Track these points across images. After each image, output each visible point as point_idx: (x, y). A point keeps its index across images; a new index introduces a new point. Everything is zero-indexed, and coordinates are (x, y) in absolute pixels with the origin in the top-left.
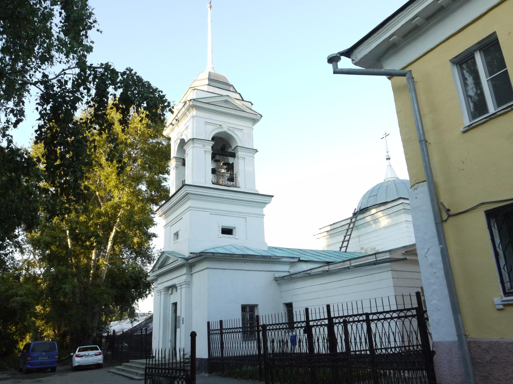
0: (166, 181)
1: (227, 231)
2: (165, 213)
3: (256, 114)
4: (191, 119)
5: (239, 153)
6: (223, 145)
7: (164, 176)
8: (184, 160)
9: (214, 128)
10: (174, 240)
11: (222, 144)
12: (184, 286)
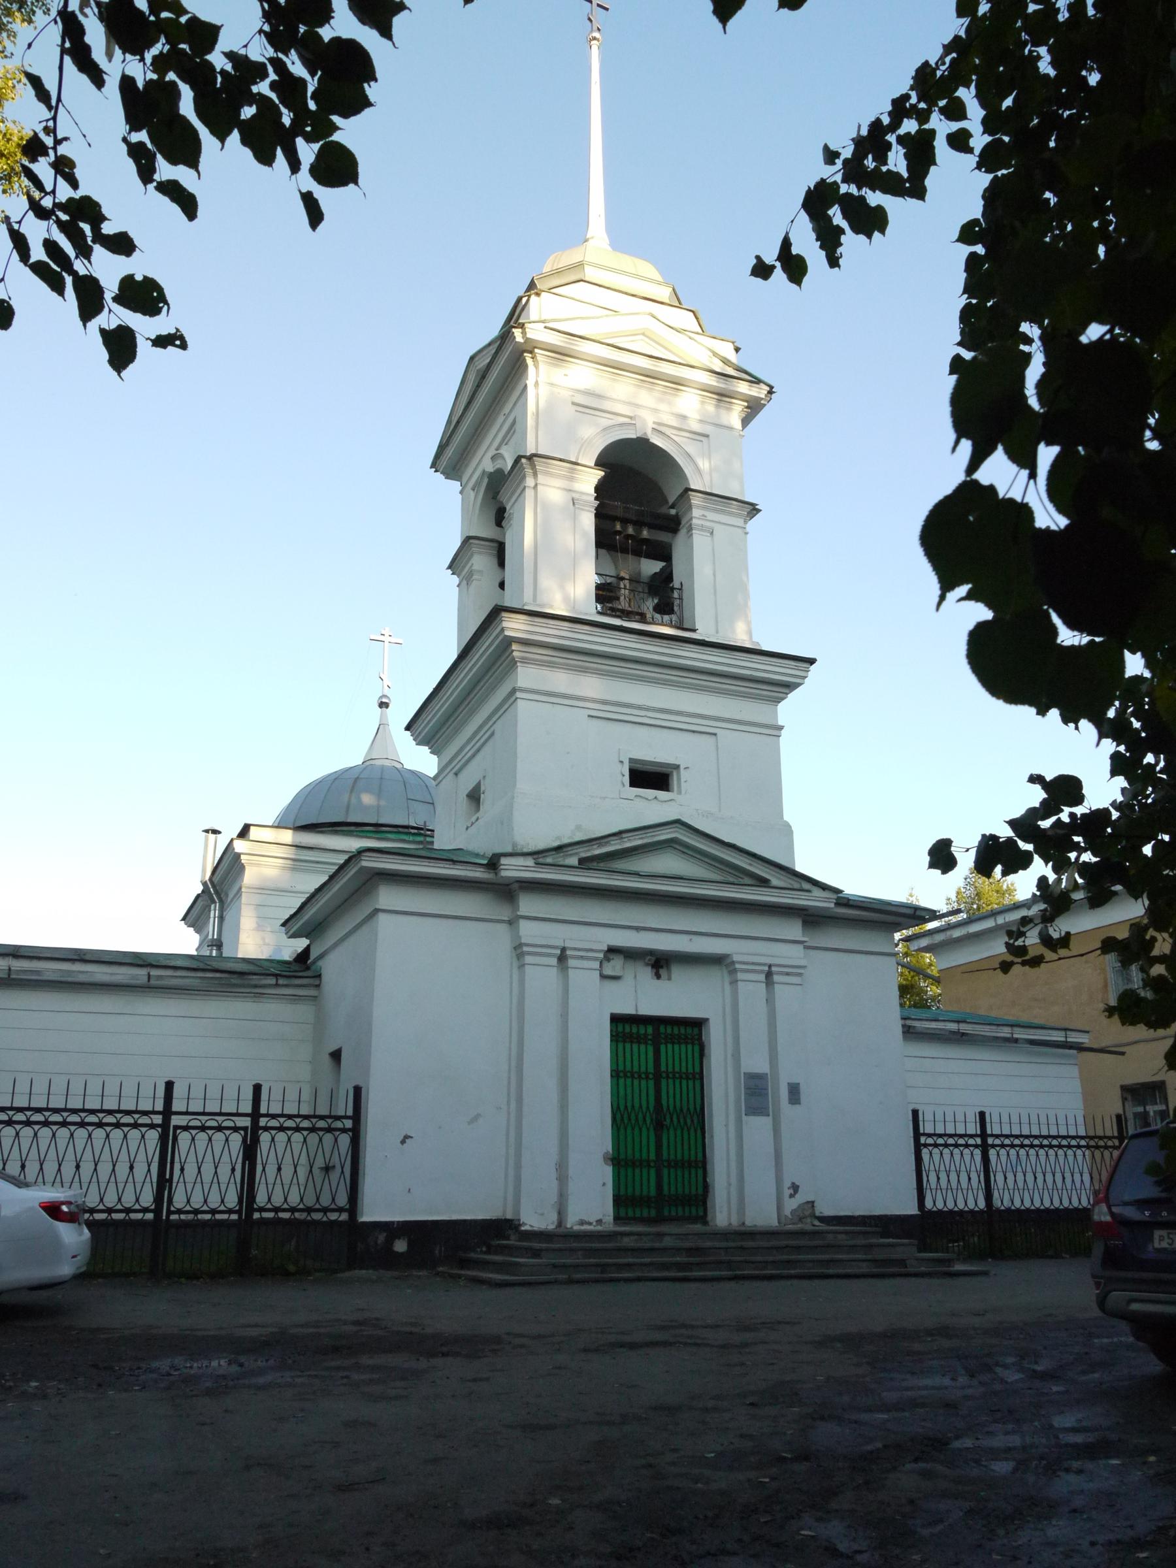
1: (651, 778)
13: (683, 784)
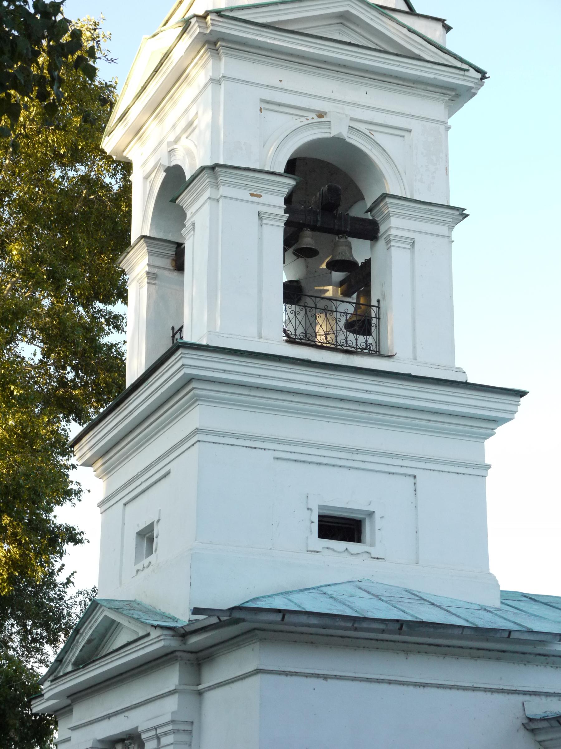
0: (118, 328)
1: (341, 528)
2: (105, 452)
3: (463, 65)
4: (210, 88)
5: (394, 221)
6: (330, 189)
7: (110, 308)
8: (179, 250)
9: (297, 123)
10: (138, 559)
11: (325, 188)
12: (169, 739)
13: (377, 532)
